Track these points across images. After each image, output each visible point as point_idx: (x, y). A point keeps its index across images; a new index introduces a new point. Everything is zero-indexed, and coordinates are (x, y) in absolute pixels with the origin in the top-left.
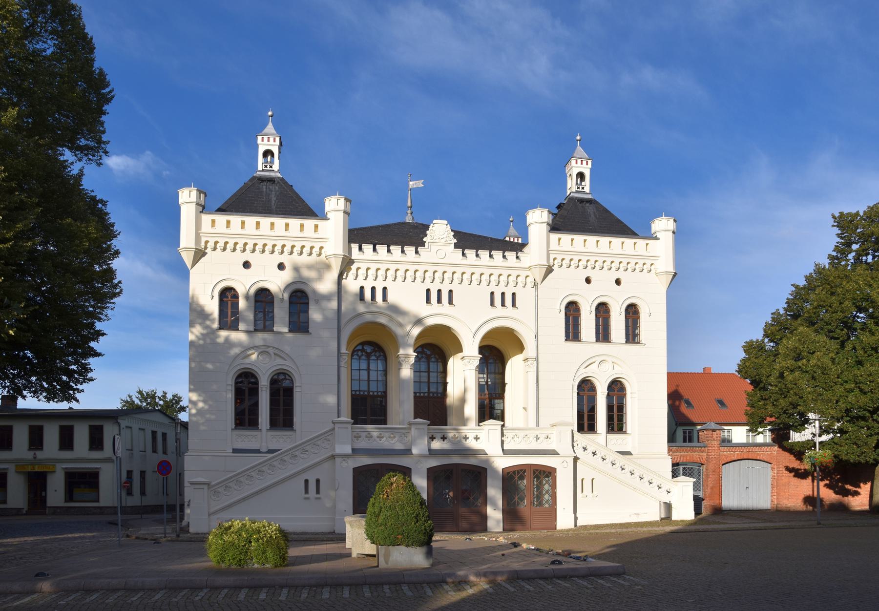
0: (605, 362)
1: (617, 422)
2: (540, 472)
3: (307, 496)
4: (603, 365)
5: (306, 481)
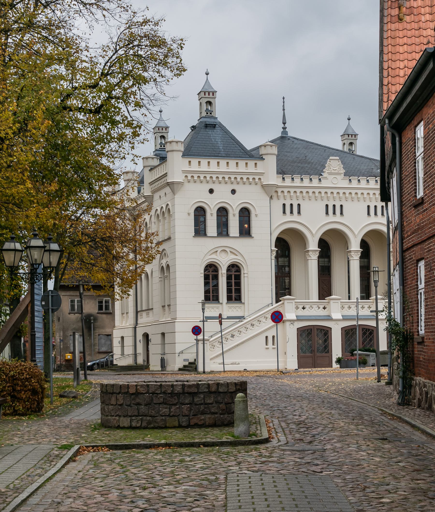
0: (222, 251)
1: (235, 294)
2: (366, 330)
3: (267, 347)
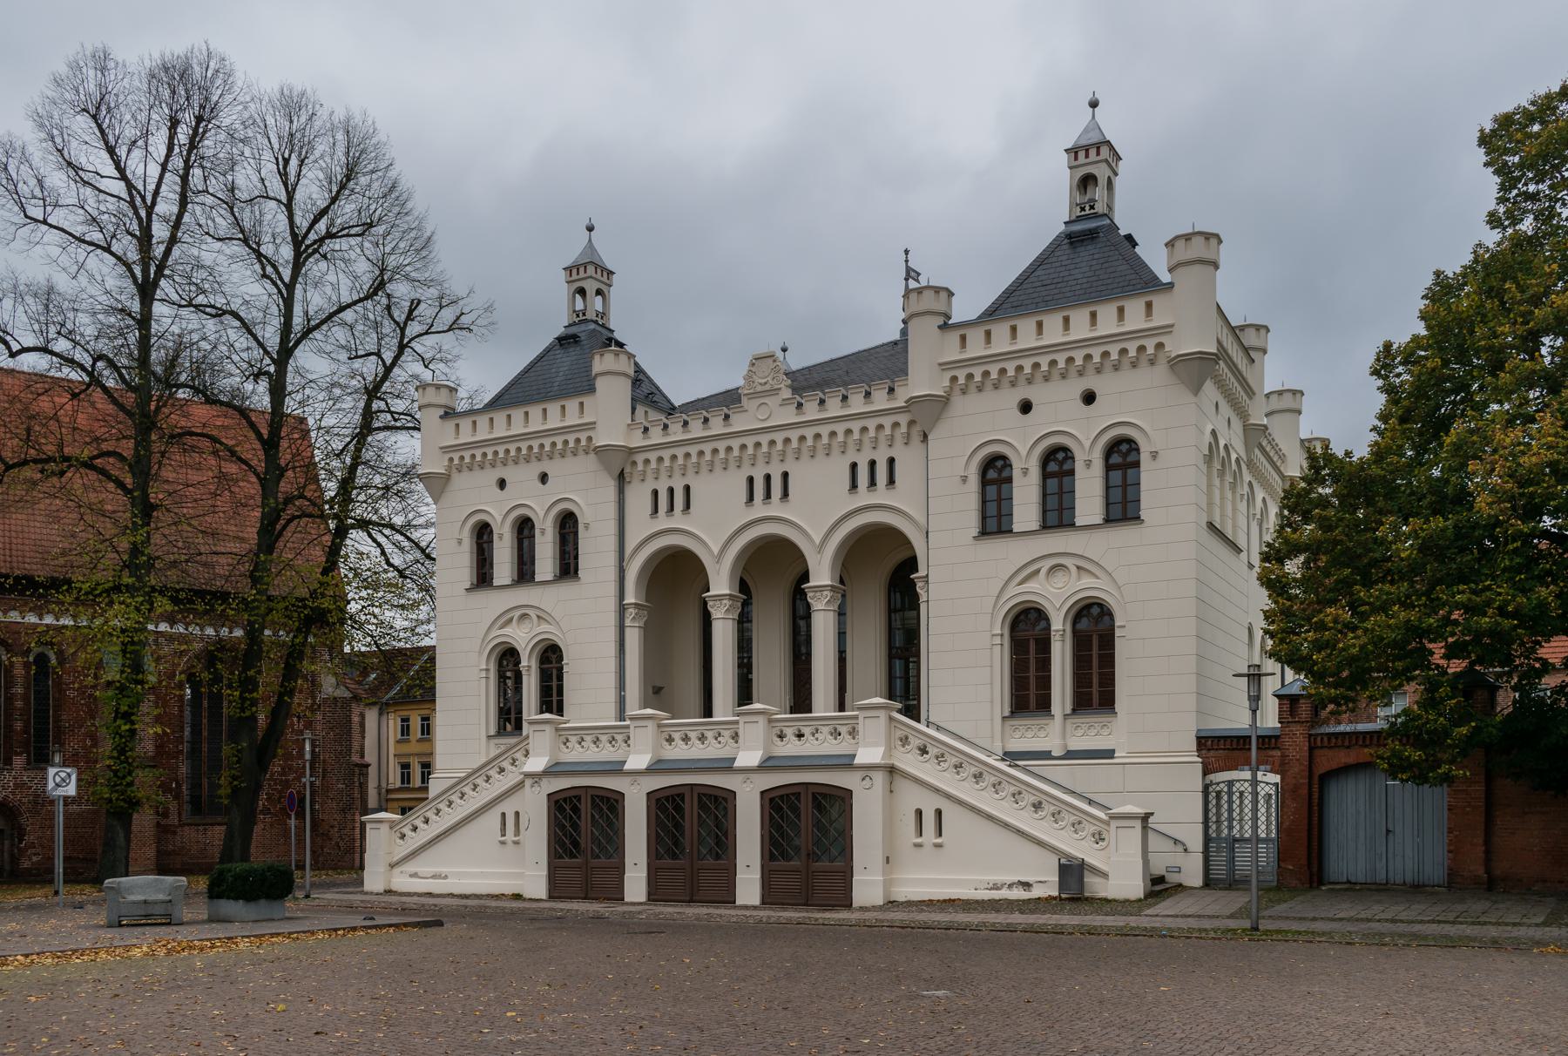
4: (1060, 574)
5: (504, 815)
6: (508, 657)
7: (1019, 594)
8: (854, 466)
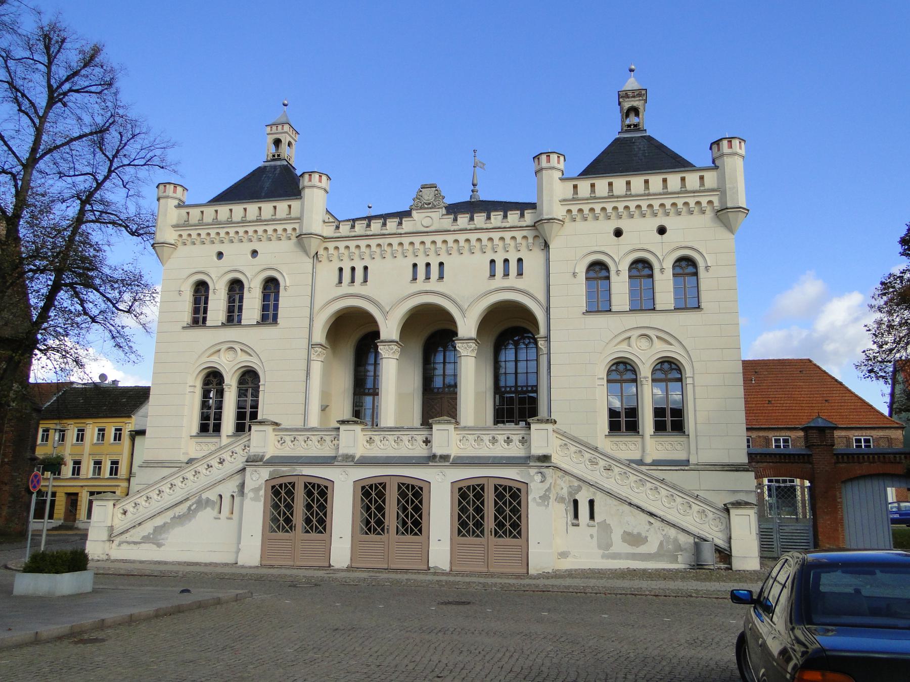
4: (231, 353)
6: (213, 379)
7: (623, 351)
8: (493, 262)
